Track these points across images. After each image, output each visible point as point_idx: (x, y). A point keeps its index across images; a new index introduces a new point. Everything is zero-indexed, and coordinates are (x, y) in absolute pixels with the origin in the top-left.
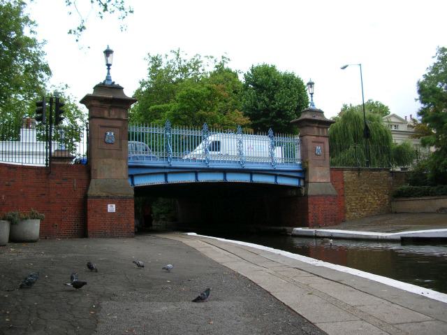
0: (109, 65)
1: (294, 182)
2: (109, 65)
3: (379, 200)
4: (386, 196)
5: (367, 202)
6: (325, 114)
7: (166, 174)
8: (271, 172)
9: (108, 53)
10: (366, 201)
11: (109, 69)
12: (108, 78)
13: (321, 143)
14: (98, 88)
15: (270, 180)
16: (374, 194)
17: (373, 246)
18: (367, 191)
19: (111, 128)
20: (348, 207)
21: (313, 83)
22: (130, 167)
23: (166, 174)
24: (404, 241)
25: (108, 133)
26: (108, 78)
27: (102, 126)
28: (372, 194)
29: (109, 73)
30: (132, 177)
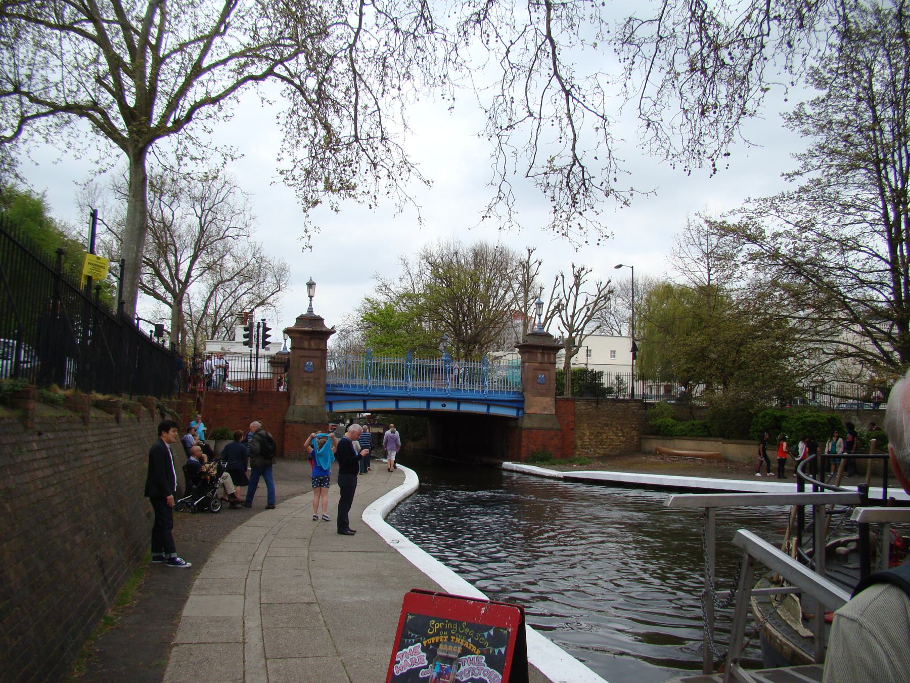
0: (311, 297)
1: (511, 413)
2: (311, 297)
3: (623, 436)
4: (634, 433)
5: (607, 438)
6: (325, 322)
7: (489, 406)
8: (349, 398)
9: (311, 285)
10: (604, 436)
11: (311, 300)
12: (310, 310)
13: (546, 370)
14: (300, 319)
15: (481, 409)
16: (617, 429)
17: (547, 480)
18: (606, 425)
19: (309, 358)
20: (579, 443)
21: (315, 284)
22: (327, 394)
23: (489, 406)
24: (566, 479)
25: (308, 363)
26: (310, 310)
27: (301, 357)
28: (614, 429)
29: (311, 303)
30: (331, 403)
